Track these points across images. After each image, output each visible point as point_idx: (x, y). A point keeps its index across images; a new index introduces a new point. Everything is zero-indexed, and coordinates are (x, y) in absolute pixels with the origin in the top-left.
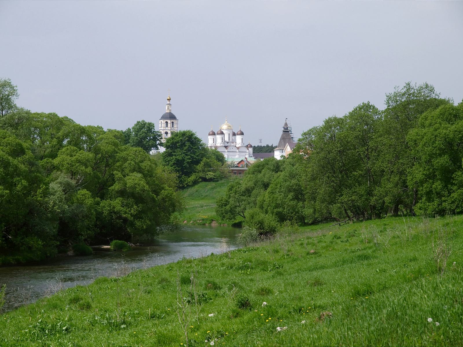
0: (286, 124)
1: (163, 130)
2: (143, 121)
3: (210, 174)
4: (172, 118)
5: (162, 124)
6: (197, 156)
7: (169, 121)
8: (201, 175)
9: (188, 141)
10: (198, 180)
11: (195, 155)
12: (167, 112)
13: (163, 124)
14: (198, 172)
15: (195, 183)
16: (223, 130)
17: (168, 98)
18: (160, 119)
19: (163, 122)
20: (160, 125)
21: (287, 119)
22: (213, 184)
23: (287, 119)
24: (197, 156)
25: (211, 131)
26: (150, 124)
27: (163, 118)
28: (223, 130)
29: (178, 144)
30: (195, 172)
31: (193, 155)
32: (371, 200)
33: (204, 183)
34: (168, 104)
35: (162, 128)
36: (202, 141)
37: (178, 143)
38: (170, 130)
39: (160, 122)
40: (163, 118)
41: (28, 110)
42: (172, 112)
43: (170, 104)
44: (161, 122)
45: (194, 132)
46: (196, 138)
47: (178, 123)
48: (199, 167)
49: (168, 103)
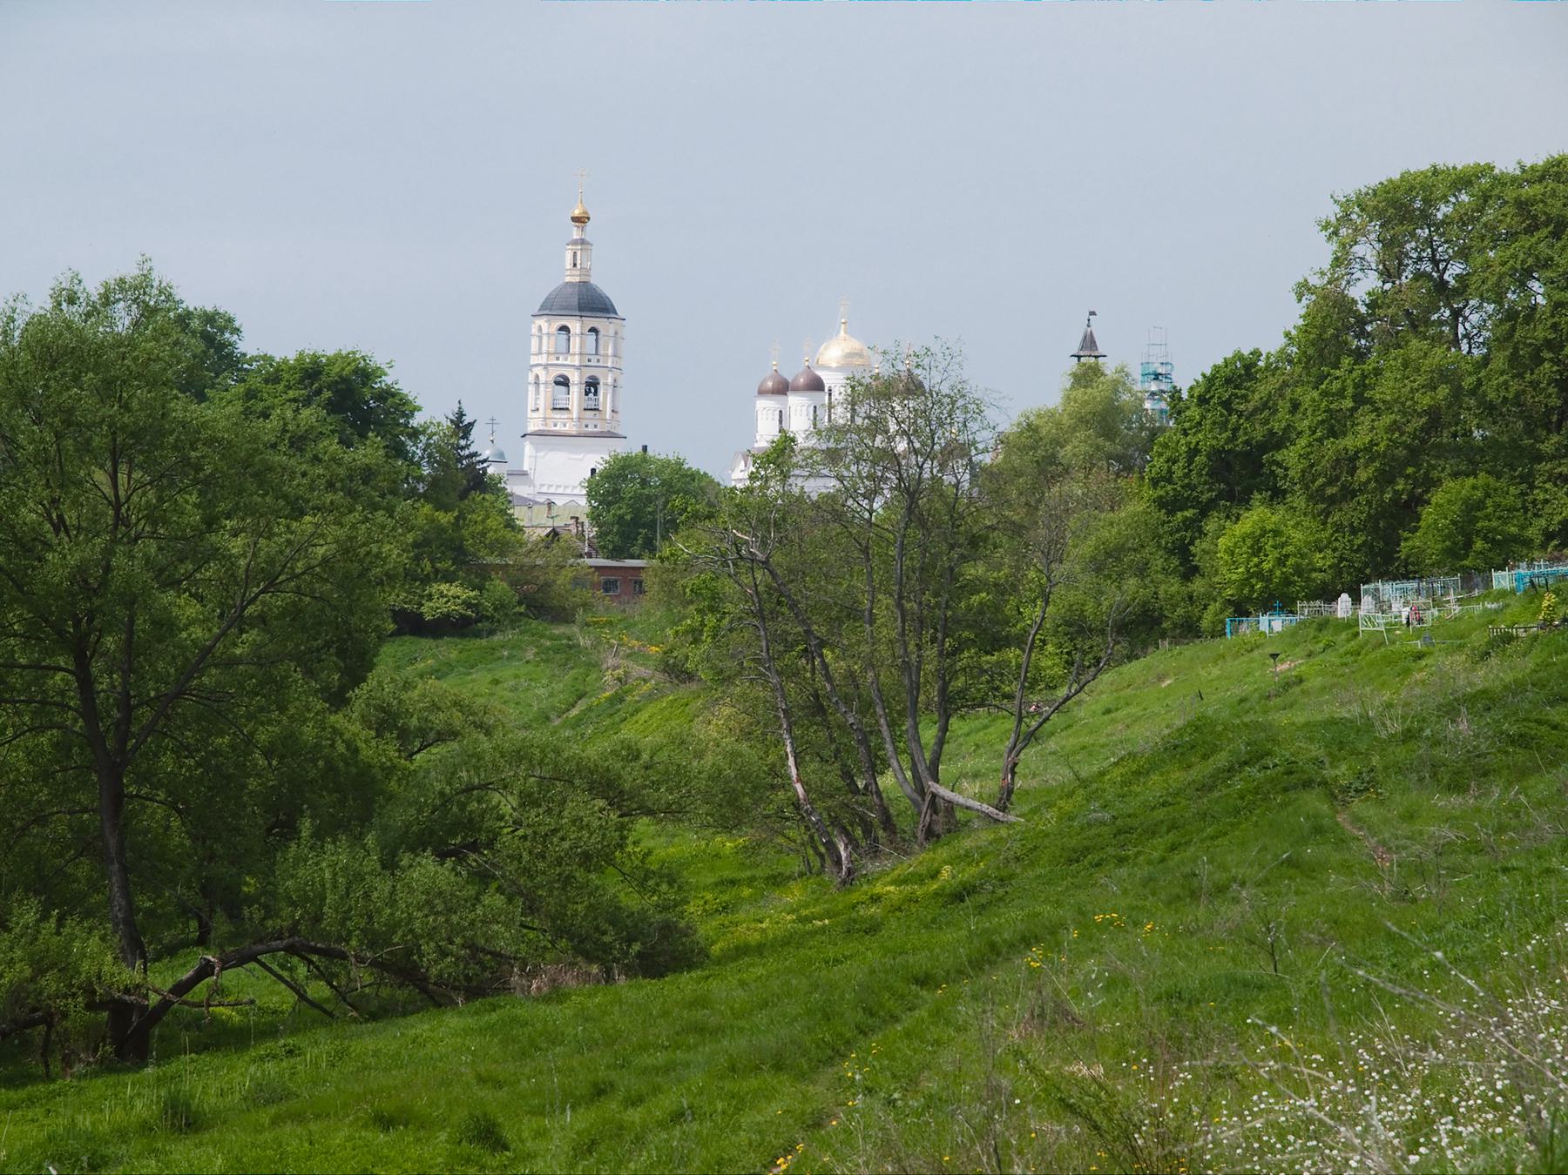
0: (1089, 342)
1: (546, 367)
3: (442, 595)
4: (593, 310)
5: (540, 338)
7: (575, 326)
12: (568, 279)
13: (545, 339)
16: (828, 368)
17: (577, 213)
18: (536, 312)
19: (548, 326)
20: (534, 342)
21: (1092, 313)
22: (449, 649)
23: (1092, 313)
25: (770, 372)
26: (210, 318)
27: (550, 307)
28: (828, 368)
32: (398, 925)
33: (408, 644)
34: (575, 242)
35: (543, 360)
36: (419, 409)
38: (578, 368)
39: (534, 331)
40: (550, 307)
41: (1246, 352)
43: (583, 242)
44: (540, 329)
45: (378, 359)
46: (387, 394)
49: (576, 234)
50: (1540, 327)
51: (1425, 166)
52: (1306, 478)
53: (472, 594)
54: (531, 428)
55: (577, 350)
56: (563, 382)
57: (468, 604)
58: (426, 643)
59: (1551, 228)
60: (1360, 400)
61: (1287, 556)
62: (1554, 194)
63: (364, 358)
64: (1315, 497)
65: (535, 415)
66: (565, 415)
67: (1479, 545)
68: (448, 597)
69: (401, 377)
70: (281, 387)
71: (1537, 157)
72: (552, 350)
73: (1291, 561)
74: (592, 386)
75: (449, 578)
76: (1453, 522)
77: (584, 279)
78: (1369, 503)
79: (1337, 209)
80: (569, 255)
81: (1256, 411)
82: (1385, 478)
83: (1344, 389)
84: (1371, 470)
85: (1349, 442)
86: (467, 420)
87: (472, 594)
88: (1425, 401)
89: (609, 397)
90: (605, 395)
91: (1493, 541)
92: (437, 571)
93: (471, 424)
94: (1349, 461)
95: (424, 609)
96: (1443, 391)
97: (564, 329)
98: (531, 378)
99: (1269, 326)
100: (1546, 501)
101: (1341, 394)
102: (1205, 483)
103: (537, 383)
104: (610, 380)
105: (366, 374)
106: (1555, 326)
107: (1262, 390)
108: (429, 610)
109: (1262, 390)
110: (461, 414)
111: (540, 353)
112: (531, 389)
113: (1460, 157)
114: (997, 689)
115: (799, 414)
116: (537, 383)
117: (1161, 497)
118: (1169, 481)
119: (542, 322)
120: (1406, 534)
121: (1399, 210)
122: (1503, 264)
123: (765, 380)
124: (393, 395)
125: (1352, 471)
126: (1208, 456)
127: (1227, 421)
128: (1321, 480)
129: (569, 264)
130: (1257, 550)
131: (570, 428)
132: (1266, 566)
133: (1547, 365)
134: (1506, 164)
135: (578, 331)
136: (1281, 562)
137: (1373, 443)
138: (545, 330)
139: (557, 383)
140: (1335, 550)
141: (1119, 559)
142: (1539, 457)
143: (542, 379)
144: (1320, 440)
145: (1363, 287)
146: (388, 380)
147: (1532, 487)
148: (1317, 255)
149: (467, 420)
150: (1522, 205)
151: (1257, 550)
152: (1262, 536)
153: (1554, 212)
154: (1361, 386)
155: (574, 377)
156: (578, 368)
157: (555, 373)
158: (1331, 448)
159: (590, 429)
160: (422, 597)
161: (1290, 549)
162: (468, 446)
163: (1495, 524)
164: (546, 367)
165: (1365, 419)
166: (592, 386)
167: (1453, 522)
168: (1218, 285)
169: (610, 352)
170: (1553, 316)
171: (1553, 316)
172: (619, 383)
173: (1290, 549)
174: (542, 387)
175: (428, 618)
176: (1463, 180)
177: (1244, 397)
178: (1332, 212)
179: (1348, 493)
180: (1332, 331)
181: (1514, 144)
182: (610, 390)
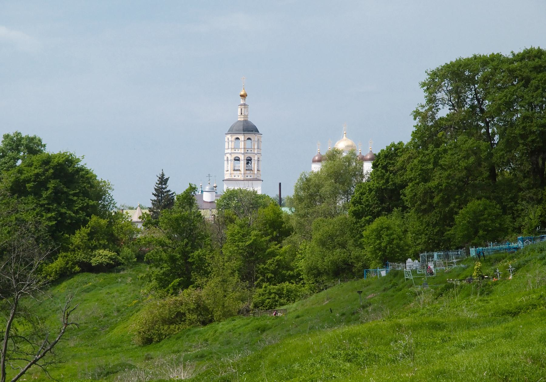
1: (231, 154)
2: (18, 134)
4: (249, 131)
6: (76, 212)
7: (242, 137)
8: (80, 256)
9: (55, 176)
10: (72, 268)
11: (69, 209)
12: (239, 119)
13: (230, 143)
14: (74, 250)
15: (64, 275)
17: (242, 93)
18: (226, 133)
20: (226, 144)
24: (76, 212)
26: (31, 140)
29: (27, 185)
30: (66, 250)
31: (63, 210)
34: (241, 105)
35: (229, 151)
37: (29, 181)
38: (243, 154)
39: (226, 140)
40: (231, 131)
41: (396, 143)
42: (249, 119)
43: (245, 105)
45: (78, 155)
47: (262, 139)
48: (78, 238)
49: (242, 102)
50: (518, 128)
51: (471, 56)
52: (413, 200)
53: (113, 254)
54: (226, 178)
55: (243, 147)
56: (237, 159)
57: (110, 258)
58: (92, 275)
59: (523, 82)
60: (436, 164)
61: (393, 239)
62: (526, 65)
63: (71, 155)
64: (418, 211)
65: (227, 172)
66: (238, 172)
67: (481, 233)
68: (103, 255)
69: (96, 163)
70: (33, 168)
71: (519, 50)
72: (233, 147)
73: (395, 242)
74: (249, 161)
75: (105, 247)
76: (469, 222)
77: (245, 119)
78: (440, 212)
79: (428, 77)
80: (239, 110)
81: (398, 170)
82: (446, 201)
83: (429, 159)
84: (439, 197)
86: (166, 177)
87: (113, 254)
88: (463, 164)
89: (256, 165)
90: (254, 164)
91: (488, 231)
92: (100, 244)
93: (167, 179)
94: (429, 193)
95: (91, 261)
96: (472, 159)
97: (238, 139)
98: (225, 159)
99: (403, 132)
100: (522, 210)
101: (428, 162)
102: (377, 203)
103: (228, 160)
104: (256, 158)
106: (524, 128)
108: (94, 261)
110: (163, 175)
111: (229, 149)
112: (226, 162)
113: (486, 51)
114: (277, 301)
116: (228, 160)
117: (355, 210)
118: (360, 203)
119: (229, 136)
120: (448, 228)
121: (458, 75)
122: (500, 99)
123: (315, 157)
124: (83, 170)
125: (432, 198)
126: (376, 192)
127: (384, 175)
128: (419, 202)
129: (239, 113)
130: (379, 237)
131: (241, 177)
132: (383, 244)
133: (521, 146)
134: (507, 53)
135: (243, 139)
136: (390, 242)
137: (440, 184)
138: (230, 139)
139: (235, 160)
140: (426, 234)
141: (333, 240)
142: (520, 189)
143: (229, 159)
144: (418, 184)
145: (444, 112)
146: (81, 164)
147: (516, 203)
148: (420, 98)
149: (166, 177)
150: (511, 71)
152: (381, 230)
153: (525, 75)
154: (437, 158)
155: (242, 157)
156: (243, 154)
157: (234, 156)
158: (422, 187)
159: (249, 177)
160: (91, 256)
161: (395, 236)
162: (166, 188)
163: (488, 222)
164: (231, 154)
165: (437, 173)
167: (469, 222)
168: (377, 115)
169: (256, 147)
170: (523, 123)
171: (523, 123)
172: (261, 159)
173: (395, 236)
174: (229, 161)
175: (93, 265)
176: (484, 61)
177: (393, 164)
178: (425, 78)
179: (431, 207)
180: (429, 134)
181: (509, 44)
182: (256, 162)
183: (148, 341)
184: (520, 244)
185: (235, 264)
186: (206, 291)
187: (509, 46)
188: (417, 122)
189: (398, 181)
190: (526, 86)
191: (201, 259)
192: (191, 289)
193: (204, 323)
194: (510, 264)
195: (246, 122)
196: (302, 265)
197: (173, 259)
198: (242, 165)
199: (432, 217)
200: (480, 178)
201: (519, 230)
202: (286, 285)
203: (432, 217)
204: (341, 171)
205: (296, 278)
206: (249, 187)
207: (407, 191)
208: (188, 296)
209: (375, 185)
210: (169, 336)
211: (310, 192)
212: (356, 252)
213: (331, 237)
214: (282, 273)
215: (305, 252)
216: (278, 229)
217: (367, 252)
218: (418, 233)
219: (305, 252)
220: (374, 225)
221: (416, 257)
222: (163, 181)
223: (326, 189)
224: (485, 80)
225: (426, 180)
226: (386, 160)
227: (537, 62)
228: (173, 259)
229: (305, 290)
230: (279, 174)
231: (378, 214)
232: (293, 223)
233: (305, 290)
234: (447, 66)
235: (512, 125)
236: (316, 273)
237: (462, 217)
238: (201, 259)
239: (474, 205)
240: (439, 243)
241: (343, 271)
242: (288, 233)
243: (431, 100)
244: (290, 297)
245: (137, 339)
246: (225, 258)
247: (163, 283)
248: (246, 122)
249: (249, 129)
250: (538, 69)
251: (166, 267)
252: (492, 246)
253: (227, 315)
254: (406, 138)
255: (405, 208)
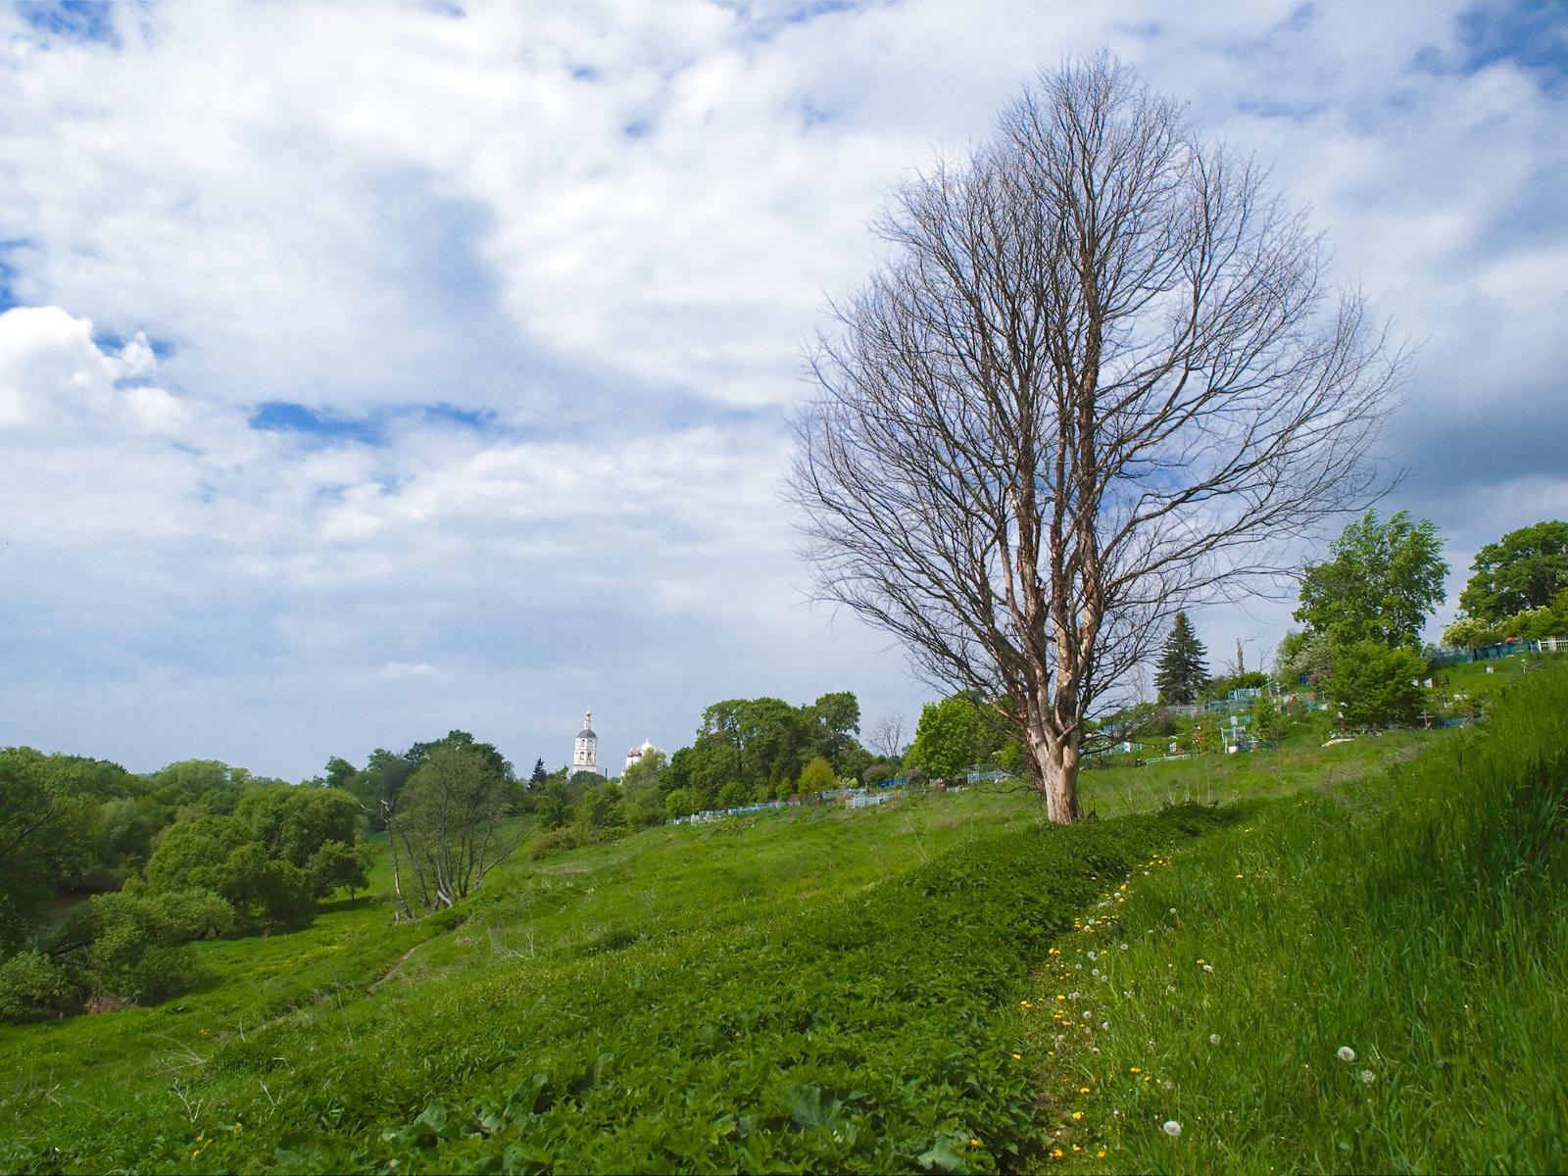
45: (494, 745)
51: (729, 699)
52: (695, 782)
64: (697, 787)
71: (757, 698)
74: (589, 754)
82: (714, 782)
85: (706, 772)
88: (724, 761)
94: (705, 777)
96: (730, 759)
99: (690, 741)
105: (28, 749)
107: (688, 757)
109: (688, 757)
115: (636, 759)
121: (723, 710)
130: (675, 801)
134: (750, 699)
145: (714, 731)
150: (753, 710)
151: (675, 801)
154: (710, 756)
158: (701, 773)
166: (589, 754)
176: (738, 703)
178: (705, 712)
180: (706, 743)
183: (536, 858)
184: (757, 808)
185: (590, 814)
186: (570, 830)
187: (752, 696)
188: (699, 736)
189: (686, 769)
190: (761, 717)
191: (570, 811)
192: (563, 828)
193: (571, 849)
194: (753, 819)
195: (589, 730)
196: (628, 816)
197: (552, 810)
198: (585, 756)
199: (706, 791)
200: (734, 770)
201: (755, 800)
202: (619, 828)
203: (706, 791)
204: (652, 761)
205: (624, 824)
206: (591, 770)
207: (692, 775)
208: (561, 832)
209: (672, 771)
210: (549, 856)
211: (634, 773)
212: (661, 810)
213: (647, 800)
214: (617, 821)
215: (630, 809)
216: (614, 795)
217: (668, 810)
218: (697, 801)
219: (630, 809)
220: (673, 794)
221: (696, 814)
222: (540, 763)
223: (643, 773)
224: (738, 713)
225: (703, 770)
226: (681, 756)
227: (767, 705)
228: (552, 810)
229: (629, 831)
230: (617, 767)
231: (672, 789)
232: (624, 792)
233: (629, 831)
234: (718, 705)
235: (753, 740)
236: (637, 822)
237: (724, 792)
238: (570, 811)
239: (730, 785)
240: (711, 806)
241: (653, 821)
242: (620, 797)
243: (707, 724)
244: (621, 835)
245: (530, 857)
246: (583, 810)
247: (546, 824)
248: (589, 730)
249: (591, 735)
250: (767, 709)
251: (548, 815)
252: (741, 809)
253: (584, 844)
254: (692, 746)
255: (690, 786)
